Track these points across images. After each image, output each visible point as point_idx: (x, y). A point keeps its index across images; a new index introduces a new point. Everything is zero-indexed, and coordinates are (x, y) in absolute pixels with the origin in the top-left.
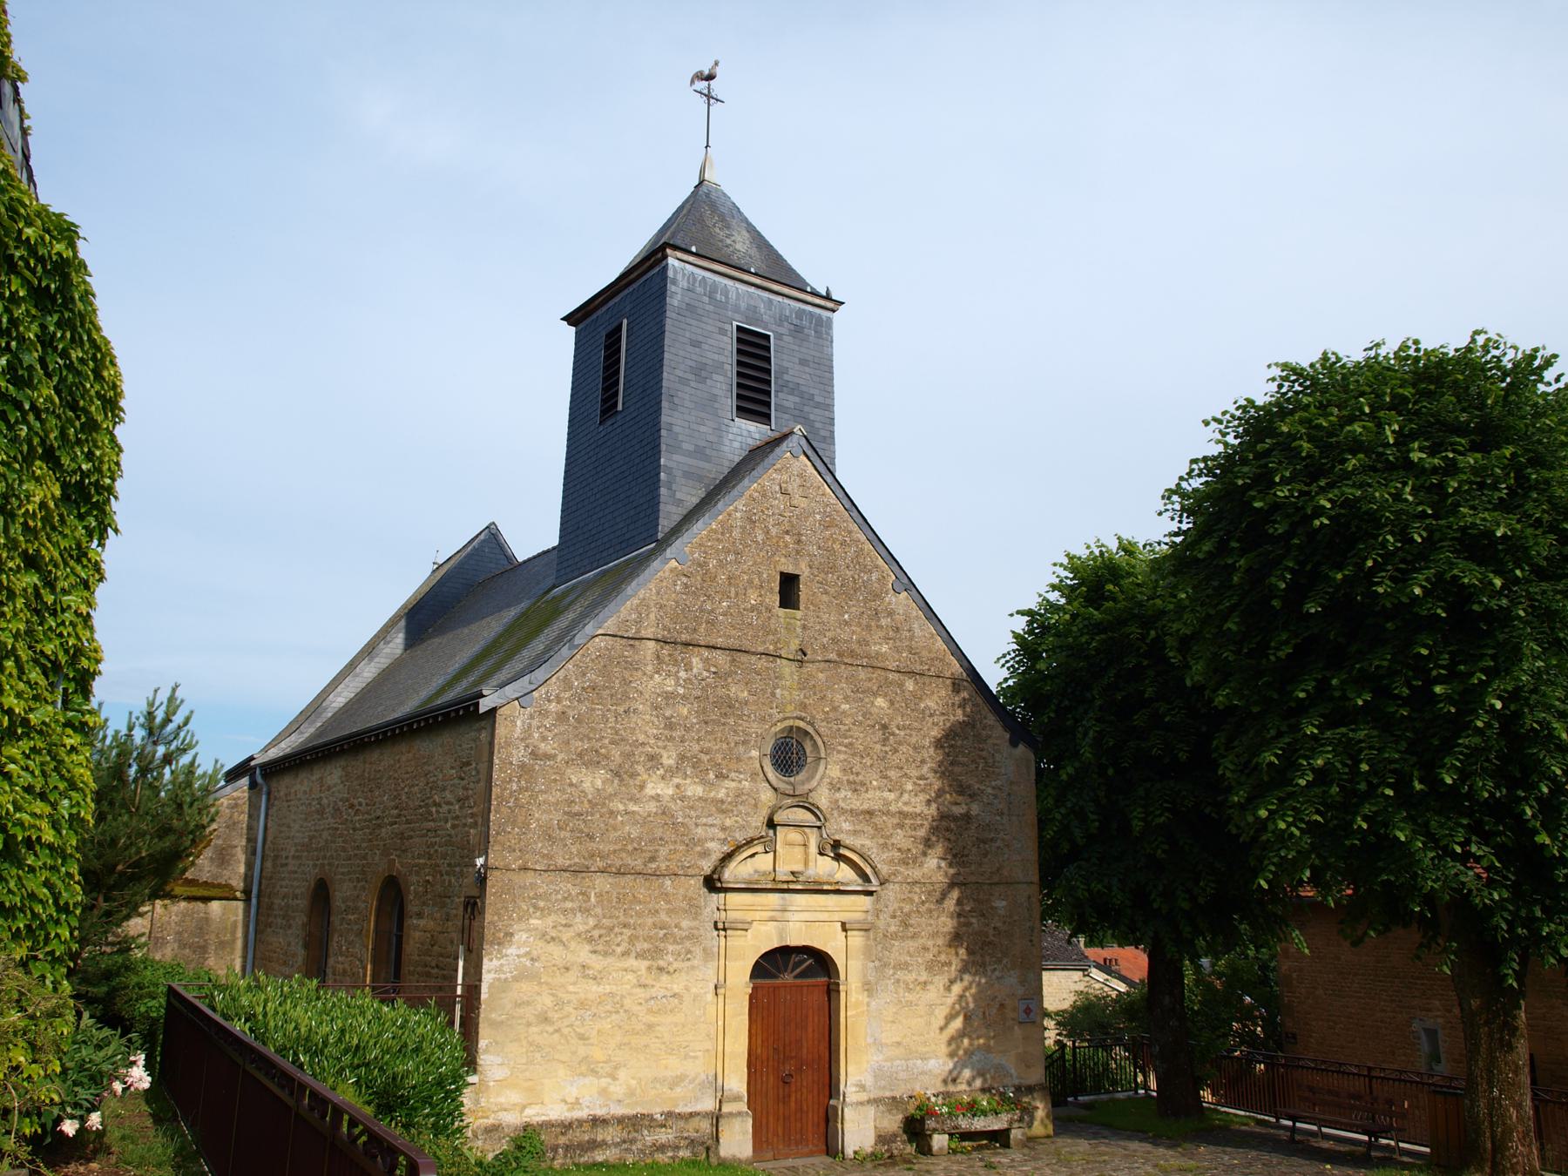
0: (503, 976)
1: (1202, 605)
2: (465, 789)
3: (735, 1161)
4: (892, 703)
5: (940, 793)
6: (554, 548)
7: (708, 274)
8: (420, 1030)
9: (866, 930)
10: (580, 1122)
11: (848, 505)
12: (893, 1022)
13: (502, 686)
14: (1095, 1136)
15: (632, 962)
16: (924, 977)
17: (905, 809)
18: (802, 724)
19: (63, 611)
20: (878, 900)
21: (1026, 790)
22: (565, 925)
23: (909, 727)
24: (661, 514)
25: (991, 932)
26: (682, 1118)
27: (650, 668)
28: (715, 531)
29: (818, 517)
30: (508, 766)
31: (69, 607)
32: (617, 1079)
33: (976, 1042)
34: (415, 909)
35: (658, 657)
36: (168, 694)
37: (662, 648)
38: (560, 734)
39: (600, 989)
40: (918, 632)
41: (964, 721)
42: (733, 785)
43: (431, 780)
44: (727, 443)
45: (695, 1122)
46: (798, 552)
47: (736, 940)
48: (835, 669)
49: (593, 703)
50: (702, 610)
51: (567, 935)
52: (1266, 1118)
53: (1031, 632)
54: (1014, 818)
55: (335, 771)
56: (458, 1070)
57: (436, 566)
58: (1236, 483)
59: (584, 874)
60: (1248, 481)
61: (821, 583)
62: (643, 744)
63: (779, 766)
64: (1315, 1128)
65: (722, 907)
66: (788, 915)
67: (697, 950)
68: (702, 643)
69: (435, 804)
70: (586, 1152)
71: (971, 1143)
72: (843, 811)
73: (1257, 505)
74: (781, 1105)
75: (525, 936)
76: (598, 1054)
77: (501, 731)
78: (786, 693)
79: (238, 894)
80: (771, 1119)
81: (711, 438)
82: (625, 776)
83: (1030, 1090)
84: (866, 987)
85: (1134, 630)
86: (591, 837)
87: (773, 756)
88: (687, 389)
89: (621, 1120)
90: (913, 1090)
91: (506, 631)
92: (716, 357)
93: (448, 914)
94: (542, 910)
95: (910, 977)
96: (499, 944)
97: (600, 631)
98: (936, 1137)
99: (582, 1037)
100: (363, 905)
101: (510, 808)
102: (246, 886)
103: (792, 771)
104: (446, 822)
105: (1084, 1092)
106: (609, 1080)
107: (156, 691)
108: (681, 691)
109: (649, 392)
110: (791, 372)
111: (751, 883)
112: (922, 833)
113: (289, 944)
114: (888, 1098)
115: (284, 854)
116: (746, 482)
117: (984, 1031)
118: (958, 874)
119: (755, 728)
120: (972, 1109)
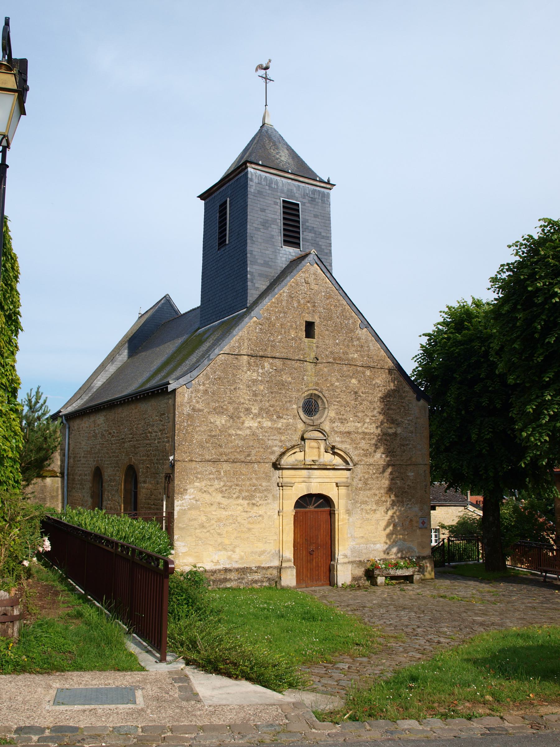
0: (183, 508)
1: (504, 336)
2: (163, 425)
3: (288, 587)
4: (359, 381)
5: (382, 423)
6: (198, 308)
7: (268, 175)
8: (150, 531)
9: (347, 486)
10: (220, 571)
11: (338, 287)
12: (360, 527)
13: (178, 379)
14: (455, 579)
15: (240, 501)
16: (374, 507)
17: (366, 431)
18: (316, 392)
19: (6, 365)
20: (353, 473)
21: (424, 421)
22: (210, 485)
23: (368, 393)
24: (249, 295)
25: (406, 487)
26: (264, 569)
27: (245, 368)
28: (274, 303)
29: (323, 294)
30: (182, 415)
31: (9, 363)
32: (235, 552)
33: (399, 536)
34: (142, 479)
35: (249, 363)
36: (36, 390)
37: (251, 359)
38: (205, 400)
39: (227, 513)
40: (372, 348)
41: (394, 389)
42: (285, 421)
43: (147, 421)
44: (279, 258)
45: (270, 571)
46: (314, 311)
47: (287, 491)
48: (332, 366)
49: (219, 385)
50: (269, 341)
51: (211, 490)
52: (536, 572)
53: (430, 344)
54: (418, 434)
55: (101, 417)
56: (167, 547)
57: (140, 315)
58: (520, 277)
59: (218, 463)
60: (526, 277)
61: (325, 325)
62: (243, 403)
63: (306, 412)
64: (556, 576)
65: (281, 476)
66: (311, 480)
67: (270, 496)
68: (269, 356)
69: (149, 432)
70: (222, 583)
71: (396, 581)
72: (336, 432)
73: (530, 289)
74: (309, 563)
75: (192, 490)
76: (227, 542)
77: (178, 399)
78: (309, 378)
79: (58, 474)
80: (304, 570)
81: (271, 256)
82: (235, 418)
83: (424, 558)
84: (347, 512)
85: (476, 344)
86: (221, 446)
87: (303, 407)
88: (259, 233)
89: (237, 570)
90: (369, 558)
91: (177, 350)
92: (273, 216)
93: (158, 481)
94: (200, 479)
95: (368, 507)
96: (181, 494)
97: (222, 352)
98: (379, 578)
99: (219, 534)
100: (118, 478)
101: (184, 434)
102: (61, 470)
103: (312, 414)
104: (155, 440)
105: (453, 561)
106: (231, 552)
107: (31, 390)
108: (260, 378)
109: (241, 235)
110: (310, 221)
111: (293, 466)
112: (373, 442)
113: (84, 497)
114: (358, 561)
115: (78, 456)
116: (288, 278)
117: (402, 532)
118: (391, 460)
119: (295, 395)
120: (396, 566)
